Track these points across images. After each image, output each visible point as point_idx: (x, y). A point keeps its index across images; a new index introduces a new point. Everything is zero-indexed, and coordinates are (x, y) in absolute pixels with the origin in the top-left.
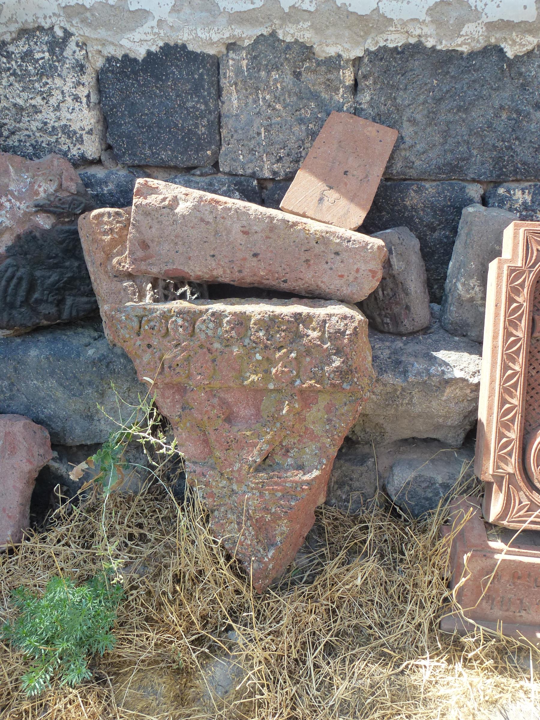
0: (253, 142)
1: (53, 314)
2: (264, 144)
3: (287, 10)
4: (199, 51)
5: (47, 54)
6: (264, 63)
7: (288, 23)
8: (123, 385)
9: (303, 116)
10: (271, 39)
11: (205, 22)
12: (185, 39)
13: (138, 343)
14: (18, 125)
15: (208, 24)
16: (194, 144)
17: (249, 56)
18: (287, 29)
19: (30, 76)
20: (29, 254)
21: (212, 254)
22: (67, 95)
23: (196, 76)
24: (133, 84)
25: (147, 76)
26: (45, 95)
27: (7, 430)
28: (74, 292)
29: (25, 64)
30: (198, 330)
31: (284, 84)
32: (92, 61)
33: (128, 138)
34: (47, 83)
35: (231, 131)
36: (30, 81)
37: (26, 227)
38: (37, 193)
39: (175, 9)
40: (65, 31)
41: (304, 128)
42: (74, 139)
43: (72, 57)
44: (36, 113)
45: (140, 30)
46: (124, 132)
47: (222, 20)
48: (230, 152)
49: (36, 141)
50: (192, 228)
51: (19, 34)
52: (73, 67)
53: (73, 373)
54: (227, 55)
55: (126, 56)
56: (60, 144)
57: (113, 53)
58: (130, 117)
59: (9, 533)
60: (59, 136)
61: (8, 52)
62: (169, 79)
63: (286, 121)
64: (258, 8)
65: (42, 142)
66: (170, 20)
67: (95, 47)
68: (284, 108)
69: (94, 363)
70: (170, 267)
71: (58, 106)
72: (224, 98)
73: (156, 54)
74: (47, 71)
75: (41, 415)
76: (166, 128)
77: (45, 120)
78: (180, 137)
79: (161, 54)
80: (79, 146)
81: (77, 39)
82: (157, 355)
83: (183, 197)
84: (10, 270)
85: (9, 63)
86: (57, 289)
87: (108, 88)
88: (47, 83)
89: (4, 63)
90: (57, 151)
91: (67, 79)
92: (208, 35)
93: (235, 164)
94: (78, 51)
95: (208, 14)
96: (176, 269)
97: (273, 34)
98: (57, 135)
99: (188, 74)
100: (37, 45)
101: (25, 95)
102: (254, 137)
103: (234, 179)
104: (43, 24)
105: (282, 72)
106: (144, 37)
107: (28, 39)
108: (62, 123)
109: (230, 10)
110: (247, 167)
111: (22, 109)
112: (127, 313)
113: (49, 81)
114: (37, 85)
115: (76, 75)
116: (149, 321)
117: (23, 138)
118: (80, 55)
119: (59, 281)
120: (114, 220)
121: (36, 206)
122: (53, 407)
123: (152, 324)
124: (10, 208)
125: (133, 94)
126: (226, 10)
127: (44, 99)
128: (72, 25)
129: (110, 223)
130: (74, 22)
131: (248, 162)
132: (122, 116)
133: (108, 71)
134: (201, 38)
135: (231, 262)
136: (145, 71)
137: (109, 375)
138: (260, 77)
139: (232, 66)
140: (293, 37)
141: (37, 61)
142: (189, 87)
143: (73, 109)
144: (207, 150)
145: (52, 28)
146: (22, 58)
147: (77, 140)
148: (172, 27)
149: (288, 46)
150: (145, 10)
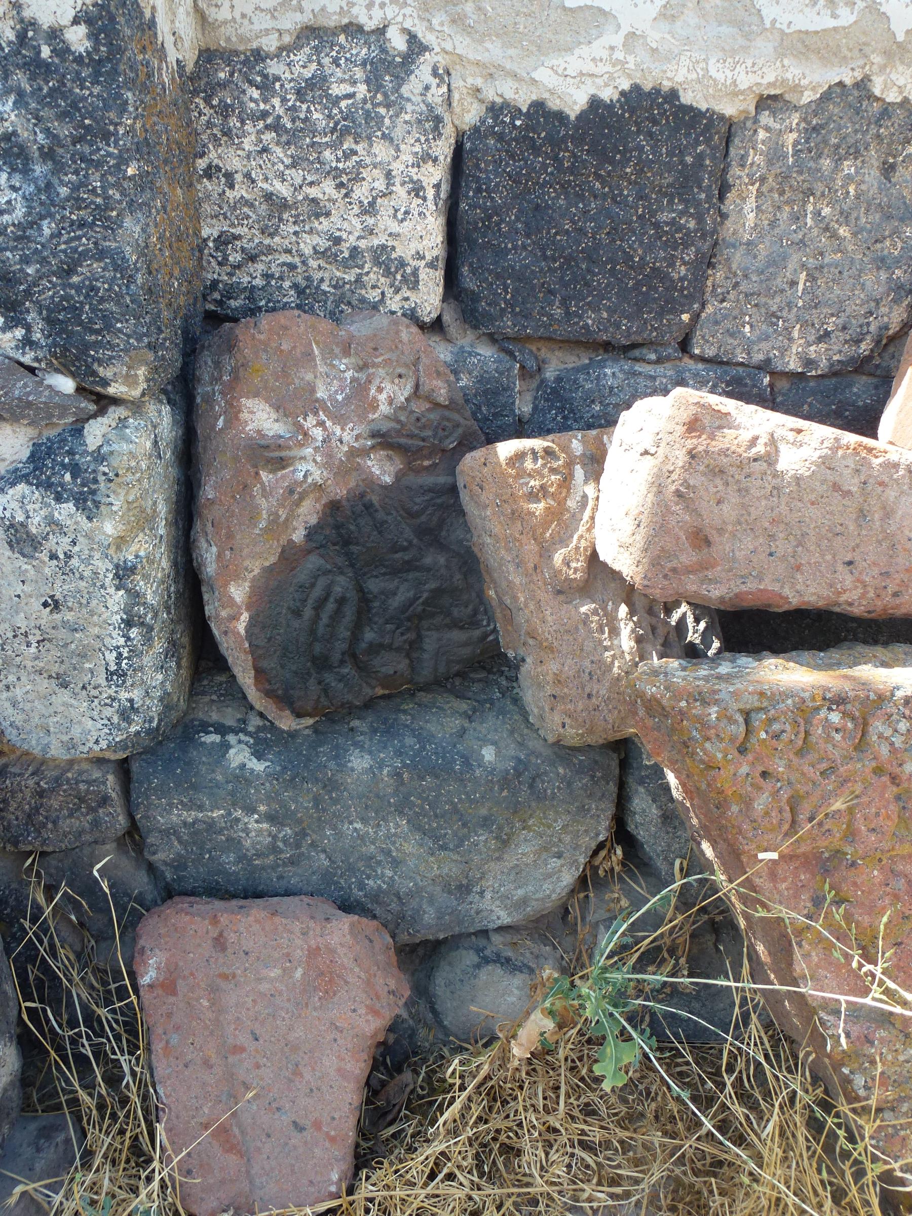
0: (778, 299)
1: (402, 675)
2: (800, 304)
3: (900, 37)
4: (703, 107)
5: (362, 90)
6: (833, 141)
7: (898, 63)
8: (556, 821)
9: (886, 252)
10: (856, 93)
11: (727, 48)
12: (679, 78)
13: (744, 769)
14: (267, 241)
15: (733, 52)
16: (659, 299)
17: (803, 125)
18: (893, 76)
19: (314, 133)
20: (357, 544)
21: (847, 559)
22: (397, 181)
23: (689, 160)
24: (544, 166)
25: (582, 151)
26: (344, 179)
27: (313, 943)
28: (438, 620)
29: (304, 107)
30: (875, 738)
31: (863, 187)
32: (457, 110)
33: (520, 280)
34: (355, 153)
35: (735, 275)
36: (313, 144)
37: (352, 484)
38: (374, 406)
39: (668, 15)
40: (412, 38)
41: (883, 276)
42: (399, 277)
43: (419, 99)
44: (317, 216)
45: (584, 51)
46: (513, 268)
47: (765, 47)
48: (725, 317)
49: (308, 279)
50: (813, 504)
51: (298, 37)
52: (419, 122)
53: (452, 803)
54: (756, 121)
55: (538, 106)
56: (364, 286)
57: (509, 95)
58: (528, 236)
59: (335, 1177)
60: (366, 270)
61: (265, 76)
62: (629, 160)
63: (852, 261)
64: (844, 28)
65: (322, 280)
66: (654, 37)
67: (470, 80)
68: (855, 234)
69: (505, 782)
70: (751, 586)
71: (372, 204)
72: (729, 205)
73: (610, 107)
74: (354, 126)
75: (355, 891)
76: (607, 263)
77: (338, 234)
78: (631, 283)
79: (622, 107)
80: (408, 294)
81: (436, 59)
82: (785, 795)
83: (791, 436)
84: (321, 583)
85: (266, 101)
86: (409, 619)
87: (486, 171)
88: (355, 153)
89: (252, 99)
90: (355, 303)
91: (403, 147)
92: (730, 75)
93: (731, 341)
94: (434, 86)
95: (736, 30)
96: (765, 590)
97: (863, 85)
98: (362, 267)
99: (670, 154)
100: (338, 65)
101: (297, 176)
102: (782, 291)
103: (726, 372)
104: (363, 19)
105: (863, 161)
106: (589, 67)
107: (317, 50)
108: (376, 242)
109: (784, 27)
110: (756, 348)
111: (284, 205)
112: (723, 705)
113: (359, 148)
114: (327, 154)
115: (423, 139)
116: (770, 721)
117: (275, 270)
118: (437, 94)
119: (412, 602)
120: (544, 465)
121: (373, 435)
122: (389, 873)
123: (776, 727)
124: (324, 441)
125: (542, 186)
126: (778, 25)
127: (341, 185)
128: (430, 28)
129: (539, 473)
130: (435, 22)
131: (760, 340)
132: (509, 231)
133: (491, 132)
134: (715, 80)
135: (886, 574)
136: (579, 140)
137: (533, 804)
138: (819, 170)
139: (763, 142)
140: (901, 93)
141: (337, 100)
142: (668, 179)
143: (407, 213)
144: (682, 312)
145: (381, 31)
146: (300, 94)
147: (405, 279)
148: (654, 51)
149: (886, 109)
150: (600, 10)
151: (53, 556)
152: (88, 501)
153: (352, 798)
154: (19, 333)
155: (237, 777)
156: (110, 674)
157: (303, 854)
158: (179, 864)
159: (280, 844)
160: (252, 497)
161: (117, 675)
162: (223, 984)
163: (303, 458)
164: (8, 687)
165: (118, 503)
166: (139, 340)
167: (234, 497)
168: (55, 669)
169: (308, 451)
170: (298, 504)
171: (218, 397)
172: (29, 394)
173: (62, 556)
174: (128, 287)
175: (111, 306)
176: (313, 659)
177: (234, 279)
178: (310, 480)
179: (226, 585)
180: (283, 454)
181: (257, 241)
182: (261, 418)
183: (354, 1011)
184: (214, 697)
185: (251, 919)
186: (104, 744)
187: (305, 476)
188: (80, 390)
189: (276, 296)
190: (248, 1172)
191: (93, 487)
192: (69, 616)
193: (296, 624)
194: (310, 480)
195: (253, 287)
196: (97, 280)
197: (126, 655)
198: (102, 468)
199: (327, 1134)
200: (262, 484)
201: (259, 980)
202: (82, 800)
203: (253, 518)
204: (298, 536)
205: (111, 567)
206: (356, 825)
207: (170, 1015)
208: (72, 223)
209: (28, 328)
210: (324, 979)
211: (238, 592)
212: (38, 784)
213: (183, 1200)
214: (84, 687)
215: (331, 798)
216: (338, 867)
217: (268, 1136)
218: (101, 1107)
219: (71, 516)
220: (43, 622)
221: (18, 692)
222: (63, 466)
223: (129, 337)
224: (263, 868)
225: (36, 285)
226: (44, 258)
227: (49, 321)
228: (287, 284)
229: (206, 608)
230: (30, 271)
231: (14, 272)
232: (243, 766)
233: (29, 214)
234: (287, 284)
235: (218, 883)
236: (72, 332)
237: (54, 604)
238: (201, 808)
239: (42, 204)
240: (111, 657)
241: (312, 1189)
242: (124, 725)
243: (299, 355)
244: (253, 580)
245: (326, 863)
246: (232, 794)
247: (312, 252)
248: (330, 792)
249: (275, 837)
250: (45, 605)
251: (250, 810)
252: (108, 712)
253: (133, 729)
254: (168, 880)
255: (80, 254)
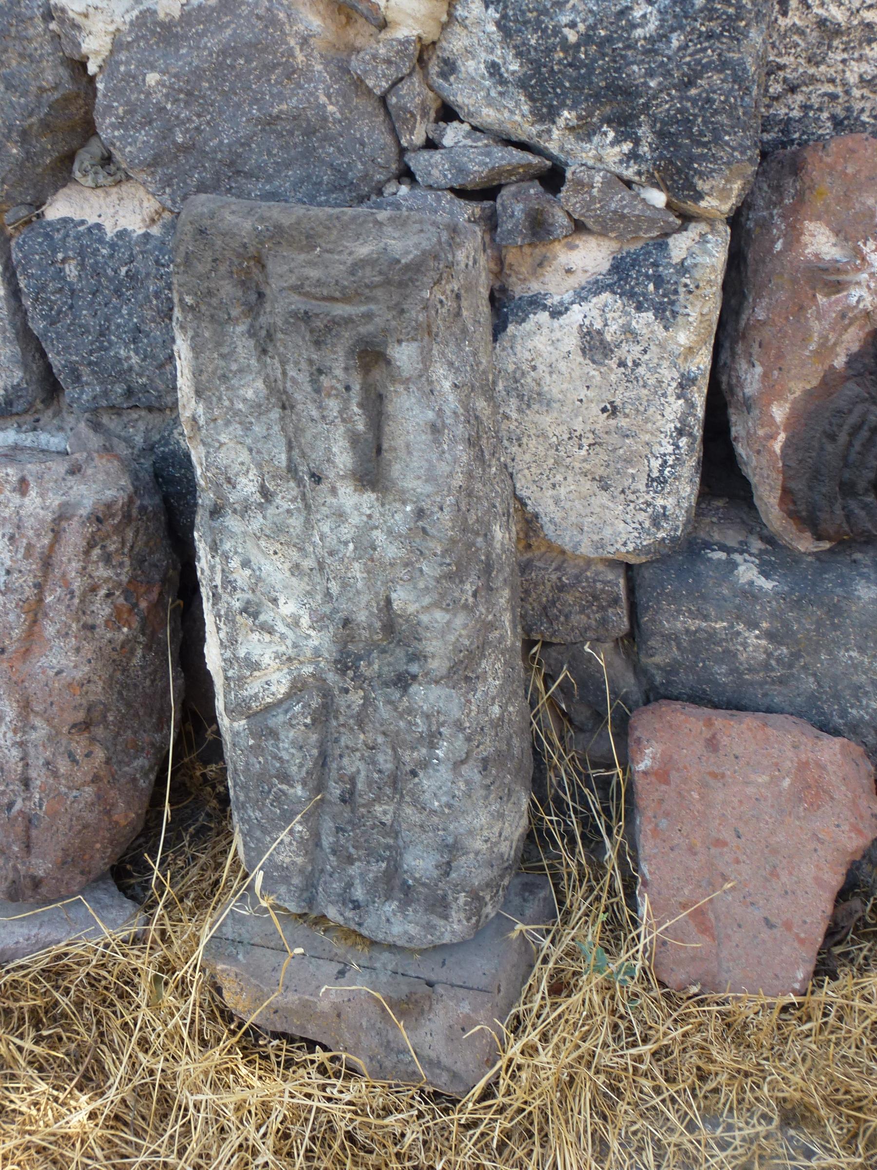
14: (812, 71)
27: (803, 757)
49: (849, 109)
59: (800, 975)
65: (863, 110)
75: (836, 718)
117: (815, 101)
151: (622, 364)
152: (666, 312)
153: (853, 626)
154: (627, 147)
155: (744, 592)
156: (651, 480)
157: (793, 675)
158: (671, 670)
159: (773, 662)
160: (807, 319)
161: (657, 482)
162: (711, 781)
163: (858, 283)
164: (554, 486)
165: (694, 315)
166: (743, 153)
167: (787, 318)
168: (601, 471)
169: (864, 276)
170: (845, 329)
171: (777, 220)
172: (624, 207)
173: (630, 364)
174: (742, 99)
175: (723, 119)
176: (841, 484)
177: (771, 111)
178: (861, 306)
179: (769, 404)
180: (841, 278)
181: (801, 70)
182: (820, 242)
183: (838, 826)
184: (714, 520)
185: (744, 726)
186: (631, 547)
187: (858, 302)
188: (669, 205)
189: (813, 128)
190: (717, 955)
191: (673, 298)
192: (623, 422)
193: (830, 447)
194: (861, 306)
195: (790, 119)
196: (714, 92)
197: (670, 462)
198: (684, 280)
199: (797, 935)
200: (817, 306)
201: (747, 783)
202: (596, 598)
203: (806, 340)
204: (839, 362)
205: (676, 375)
206: (852, 654)
207: (661, 801)
208: (701, 34)
209: (637, 142)
210: (810, 791)
211: (779, 412)
212: (560, 579)
213: (655, 967)
214: (623, 492)
215: (833, 624)
216: (825, 692)
217: (740, 926)
218: (581, 876)
219: (648, 325)
220: (598, 426)
221: (563, 491)
222: (647, 277)
223: (734, 149)
224: (752, 684)
225: (655, 97)
226: (668, 71)
227: (661, 135)
228: (825, 115)
229: (733, 429)
230: (652, 84)
231: (637, 86)
232: (751, 583)
233: (661, 27)
234: (825, 115)
235: (704, 691)
236: (680, 146)
237: (612, 410)
238: (706, 618)
239: (675, 16)
240: (656, 464)
241: (776, 982)
242: (653, 530)
243: (863, 178)
244: (794, 402)
245: (814, 687)
246: (738, 608)
247: (857, 80)
248: (833, 617)
249: (770, 655)
250: (604, 410)
251: (753, 625)
252: (642, 516)
253: (661, 535)
254: (657, 683)
255: (703, 66)
